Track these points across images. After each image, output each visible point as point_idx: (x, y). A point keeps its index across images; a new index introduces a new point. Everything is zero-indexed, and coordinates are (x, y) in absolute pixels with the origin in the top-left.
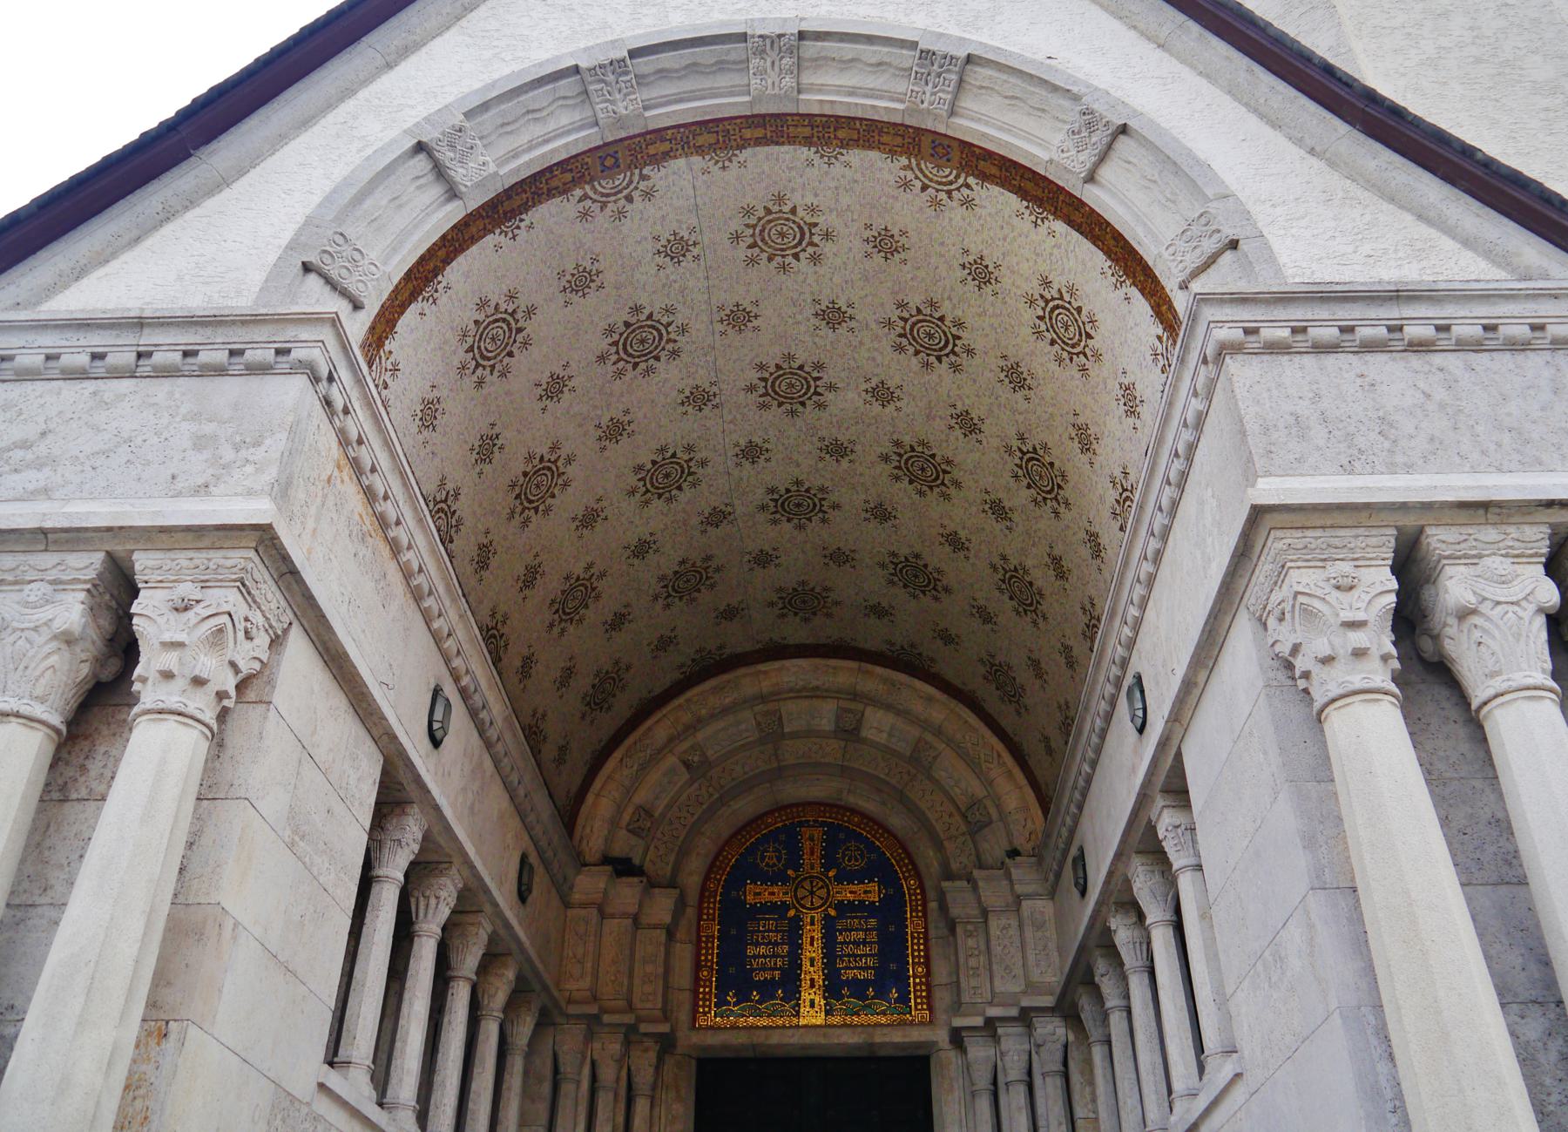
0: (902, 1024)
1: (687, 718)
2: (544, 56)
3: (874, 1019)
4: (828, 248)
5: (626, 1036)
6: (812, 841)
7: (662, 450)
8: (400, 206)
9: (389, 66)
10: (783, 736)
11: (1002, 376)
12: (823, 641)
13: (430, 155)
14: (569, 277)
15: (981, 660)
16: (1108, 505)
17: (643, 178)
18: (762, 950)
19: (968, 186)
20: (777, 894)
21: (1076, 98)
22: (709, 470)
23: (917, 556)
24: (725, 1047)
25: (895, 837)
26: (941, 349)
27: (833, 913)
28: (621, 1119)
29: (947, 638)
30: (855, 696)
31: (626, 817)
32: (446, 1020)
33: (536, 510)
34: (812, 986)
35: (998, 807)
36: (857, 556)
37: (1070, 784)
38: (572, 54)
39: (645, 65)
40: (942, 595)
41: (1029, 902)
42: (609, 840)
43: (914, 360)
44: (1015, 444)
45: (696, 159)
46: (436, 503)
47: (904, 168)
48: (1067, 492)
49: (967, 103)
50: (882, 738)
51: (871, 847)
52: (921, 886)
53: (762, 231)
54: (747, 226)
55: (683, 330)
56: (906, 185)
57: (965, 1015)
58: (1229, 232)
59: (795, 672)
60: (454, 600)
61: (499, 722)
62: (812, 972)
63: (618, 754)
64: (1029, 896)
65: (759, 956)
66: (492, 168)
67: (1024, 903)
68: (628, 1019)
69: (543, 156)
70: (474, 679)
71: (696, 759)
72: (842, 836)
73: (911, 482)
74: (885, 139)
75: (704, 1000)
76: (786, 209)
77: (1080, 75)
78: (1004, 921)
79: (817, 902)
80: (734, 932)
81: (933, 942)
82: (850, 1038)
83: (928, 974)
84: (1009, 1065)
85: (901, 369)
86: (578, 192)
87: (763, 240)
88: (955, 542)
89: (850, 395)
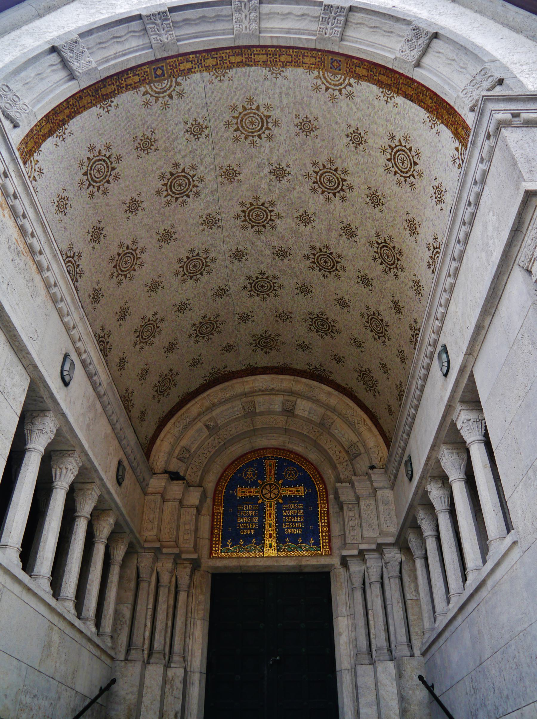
0: (316, 555)
1: (207, 403)
2: (122, 11)
3: (302, 553)
4: (276, 131)
6: (270, 466)
7: (192, 251)
8: (42, 79)
9: (40, 16)
10: (256, 414)
11: (368, 200)
12: (276, 365)
13: (59, 54)
14: (139, 141)
15: (355, 370)
16: (425, 261)
17: (178, 84)
18: (245, 519)
19: (350, 85)
20: (254, 492)
21: (408, 23)
22: (216, 264)
23: (323, 314)
24: (226, 567)
25: (312, 464)
26: (336, 189)
27: (281, 501)
28: (171, 602)
29: (338, 359)
30: (292, 393)
31: (177, 452)
32: (73, 538)
33: (125, 276)
34: (270, 537)
35: (364, 446)
36: (292, 316)
37: (403, 423)
38: (138, 10)
39: (177, 16)
40: (336, 335)
42: (167, 462)
43: (321, 197)
44: (374, 239)
45: (205, 74)
46: (67, 257)
47: (316, 78)
48: (403, 262)
49: (350, 33)
50: (306, 414)
51: (300, 469)
52: (325, 488)
53: (242, 121)
54: (234, 117)
55: (201, 180)
56: (317, 88)
58: (498, 75)
59: (262, 381)
60: (76, 308)
61: (105, 384)
62: (270, 529)
63: (172, 421)
64: (381, 489)
65: (244, 523)
66: (94, 65)
67: (378, 492)
68: (176, 551)
69: (122, 62)
70: (89, 356)
71: (212, 424)
72: (285, 464)
73: (320, 270)
74: (306, 60)
75: (216, 544)
76: (254, 107)
77: (411, 13)
78: (367, 502)
79: (273, 496)
80: (231, 511)
81: (331, 515)
82: (290, 563)
83: (329, 531)
84: (371, 574)
85: (314, 203)
86: (142, 89)
87: (242, 126)
88: (343, 303)
89: (289, 220)
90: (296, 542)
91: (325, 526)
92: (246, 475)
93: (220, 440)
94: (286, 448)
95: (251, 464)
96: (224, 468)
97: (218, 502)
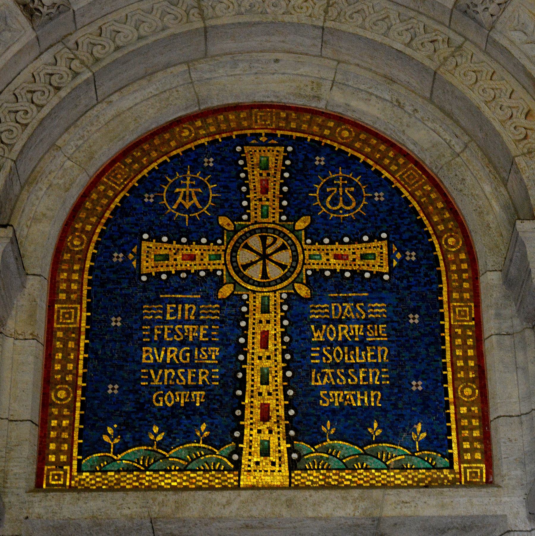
3: (383, 476)
6: (264, 169)
18: (171, 354)
20: (202, 257)
27: (303, 291)
34: (265, 417)
51: (375, 181)
52: (469, 246)
62: (265, 386)
65: (164, 365)
72: (320, 161)
75: (59, 440)
80: (116, 322)
81: (491, 345)
90: (360, 438)
91: (467, 380)
92: (172, 197)
93: (76, 64)
94: (321, 106)
95: (191, 159)
96: (93, 170)
97: (68, 291)
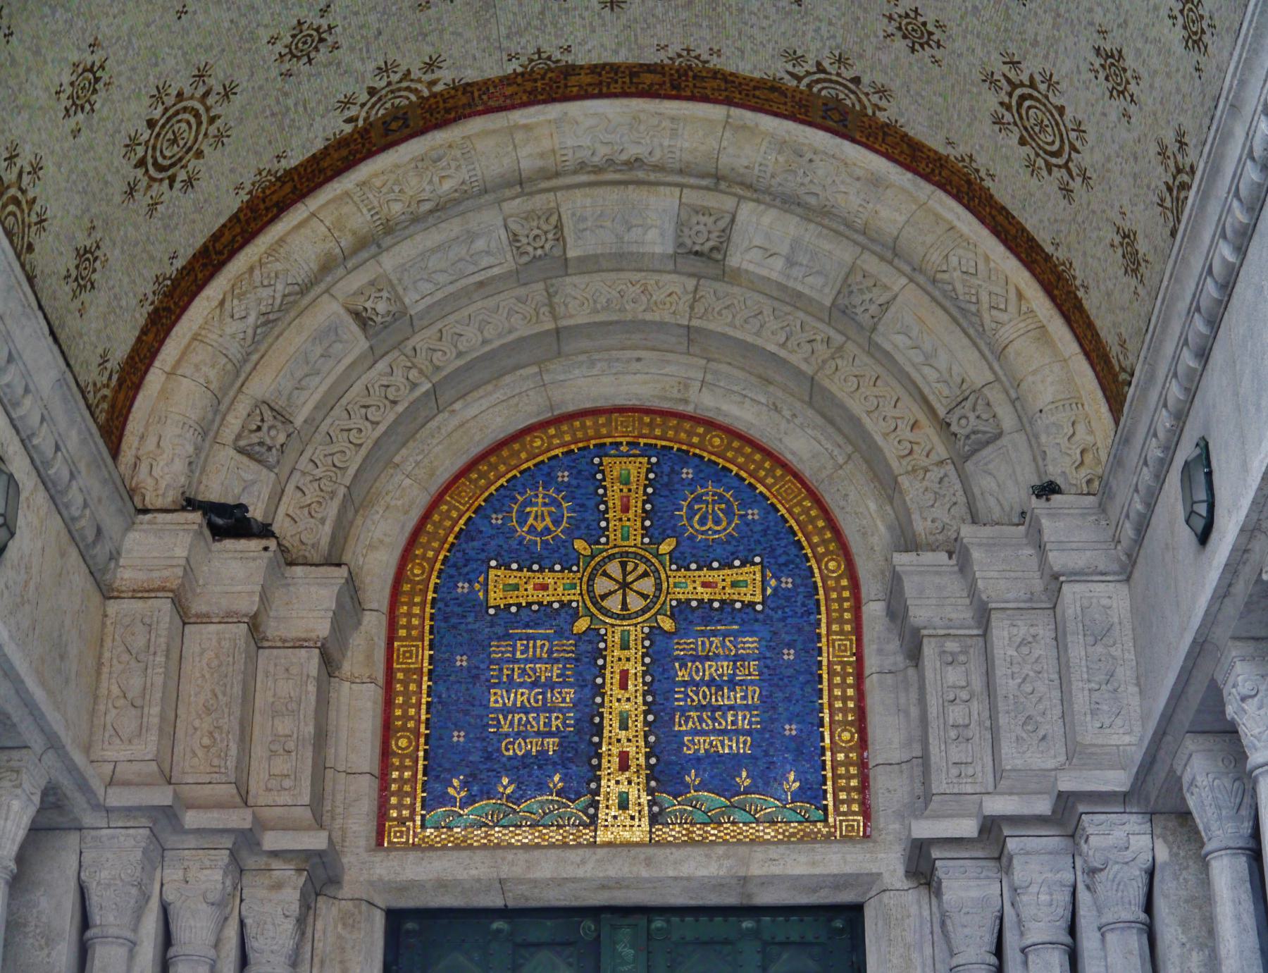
0: (808, 839)
1: (360, 221)
5: (233, 854)
6: (625, 476)
15: (990, 79)
18: (522, 696)
24: (442, 885)
31: (234, 422)
34: (624, 767)
41: (1078, 588)
50: (774, 269)
51: (748, 495)
57: (937, 816)
64: (1078, 576)
71: (381, 307)
72: (687, 473)
81: (871, 683)
83: (863, 743)
